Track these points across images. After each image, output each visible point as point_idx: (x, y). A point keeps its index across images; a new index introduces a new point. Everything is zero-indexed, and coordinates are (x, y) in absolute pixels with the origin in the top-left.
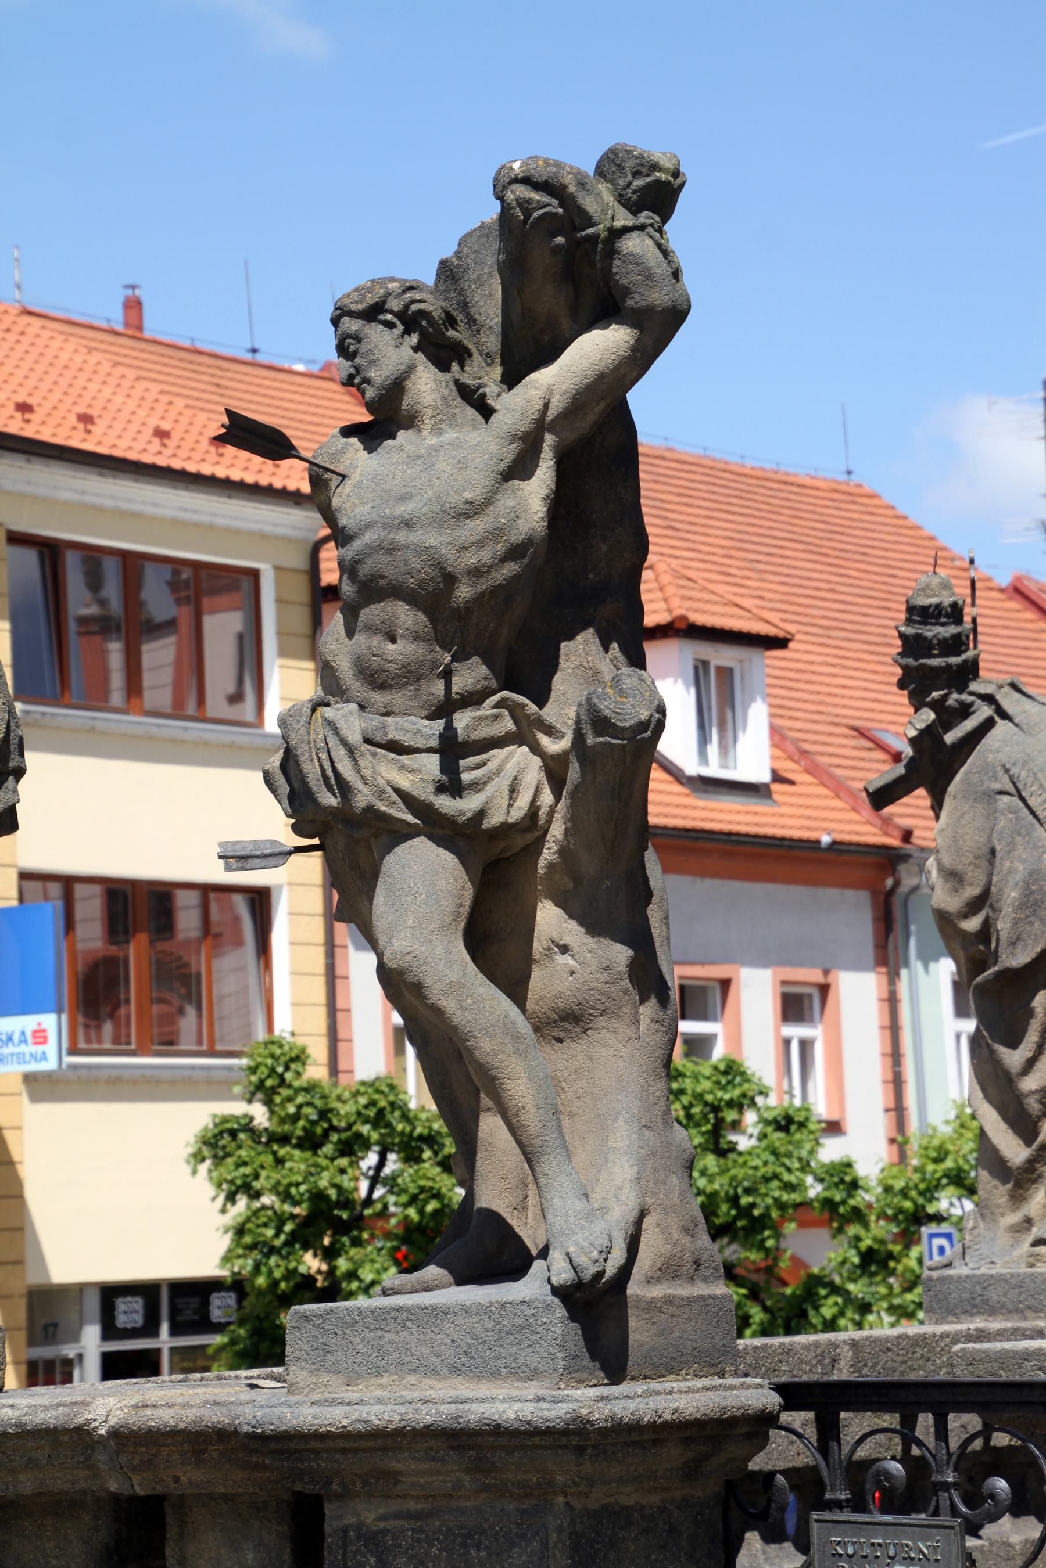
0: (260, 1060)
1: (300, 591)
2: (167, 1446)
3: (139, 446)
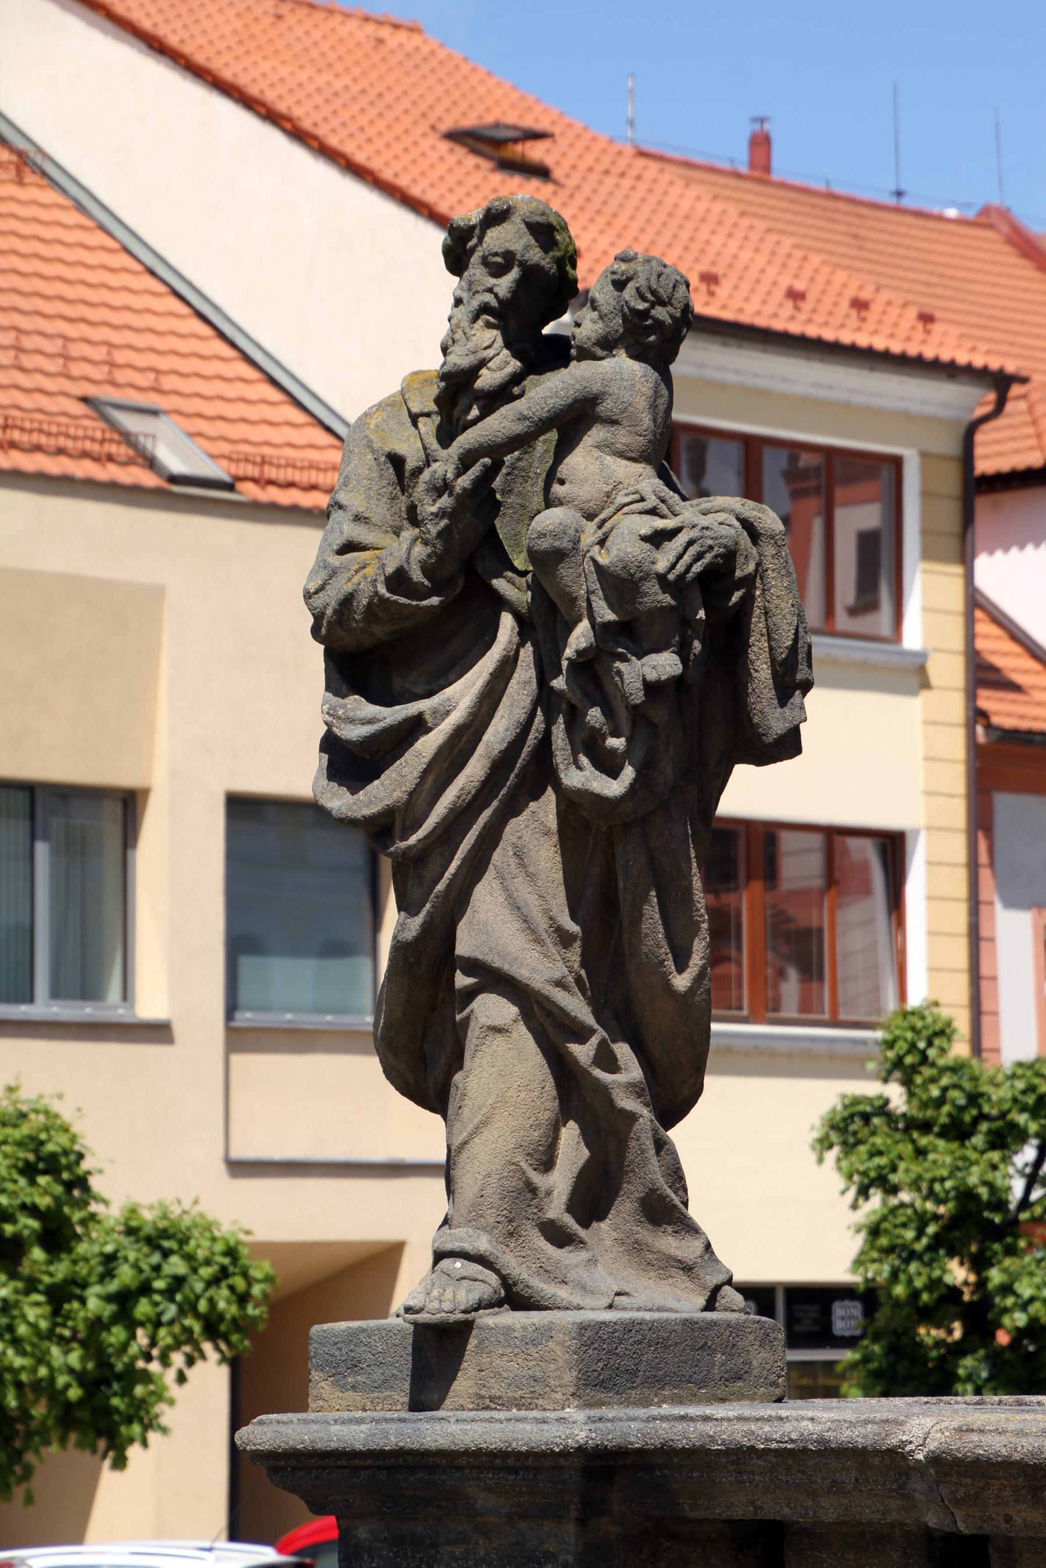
0: (898, 1032)
1: (950, 482)
2: (997, 1479)
3: (769, 310)
